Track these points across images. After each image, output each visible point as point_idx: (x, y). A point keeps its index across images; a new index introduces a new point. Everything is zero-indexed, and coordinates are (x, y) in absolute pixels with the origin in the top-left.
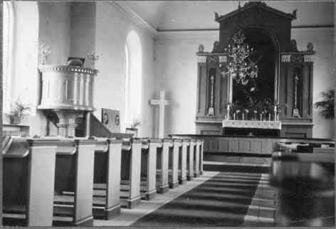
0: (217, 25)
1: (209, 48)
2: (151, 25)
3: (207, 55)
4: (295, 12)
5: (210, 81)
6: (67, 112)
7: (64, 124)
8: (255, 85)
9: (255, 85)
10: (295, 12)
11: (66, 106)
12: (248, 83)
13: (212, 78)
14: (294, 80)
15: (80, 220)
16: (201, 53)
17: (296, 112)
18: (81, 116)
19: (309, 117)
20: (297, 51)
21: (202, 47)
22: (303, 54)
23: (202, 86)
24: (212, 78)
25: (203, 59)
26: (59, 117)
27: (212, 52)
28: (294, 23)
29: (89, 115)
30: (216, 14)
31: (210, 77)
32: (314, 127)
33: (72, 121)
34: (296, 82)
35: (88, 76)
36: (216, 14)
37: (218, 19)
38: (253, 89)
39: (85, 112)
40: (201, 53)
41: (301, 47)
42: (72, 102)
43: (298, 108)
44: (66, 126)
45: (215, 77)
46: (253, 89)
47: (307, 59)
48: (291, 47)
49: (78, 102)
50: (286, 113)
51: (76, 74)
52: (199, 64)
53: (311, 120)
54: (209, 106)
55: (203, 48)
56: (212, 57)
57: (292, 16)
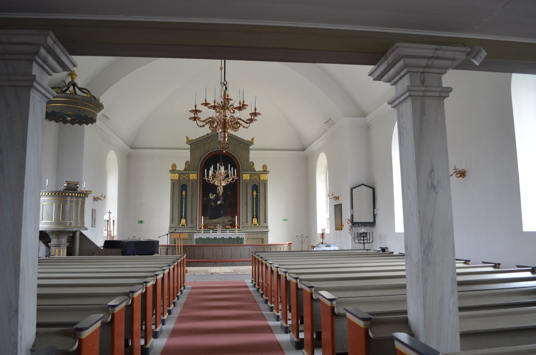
0: (189, 146)
1: (181, 167)
2: (128, 145)
3: (180, 173)
4: (253, 139)
5: (182, 195)
6: (58, 233)
7: (56, 243)
8: (221, 199)
9: (221, 199)
10: (253, 139)
11: (61, 228)
12: (215, 198)
13: (184, 193)
14: (253, 195)
15: (461, 51)
16: (173, 171)
17: (255, 220)
18: (71, 235)
19: (265, 225)
20: (255, 171)
21: (174, 166)
22: (259, 174)
23: (174, 209)
24: (184, 193)
25: (176, 176)
26: (51, 237)
27: (185, 170)
28: (251, 147)
29: (78, 234)
30: (187, 138)
31: (182, 192)
32: (269, 233)
33: (64, 240)
34: (255, 196)
35: (80, 199)
36: (187, 138)
37: (189, 142)
38: (219, 202)
39: (74, 233)
40: (173, 171)
41: (258, 168)
42: (66, 223)
43: (257, 217)
44: (58, 246)
45: (186, 192)
46: (219, 202)
47: (262, 177)
48: (250, 168)
49: (72, 224)
50: (247, 222)
51: (69, 198)
52: (172, 180)
53: (267, 227)
54: (181, 218)
55: (175, 167)
56: (184, 174)
57: (251, 142)
